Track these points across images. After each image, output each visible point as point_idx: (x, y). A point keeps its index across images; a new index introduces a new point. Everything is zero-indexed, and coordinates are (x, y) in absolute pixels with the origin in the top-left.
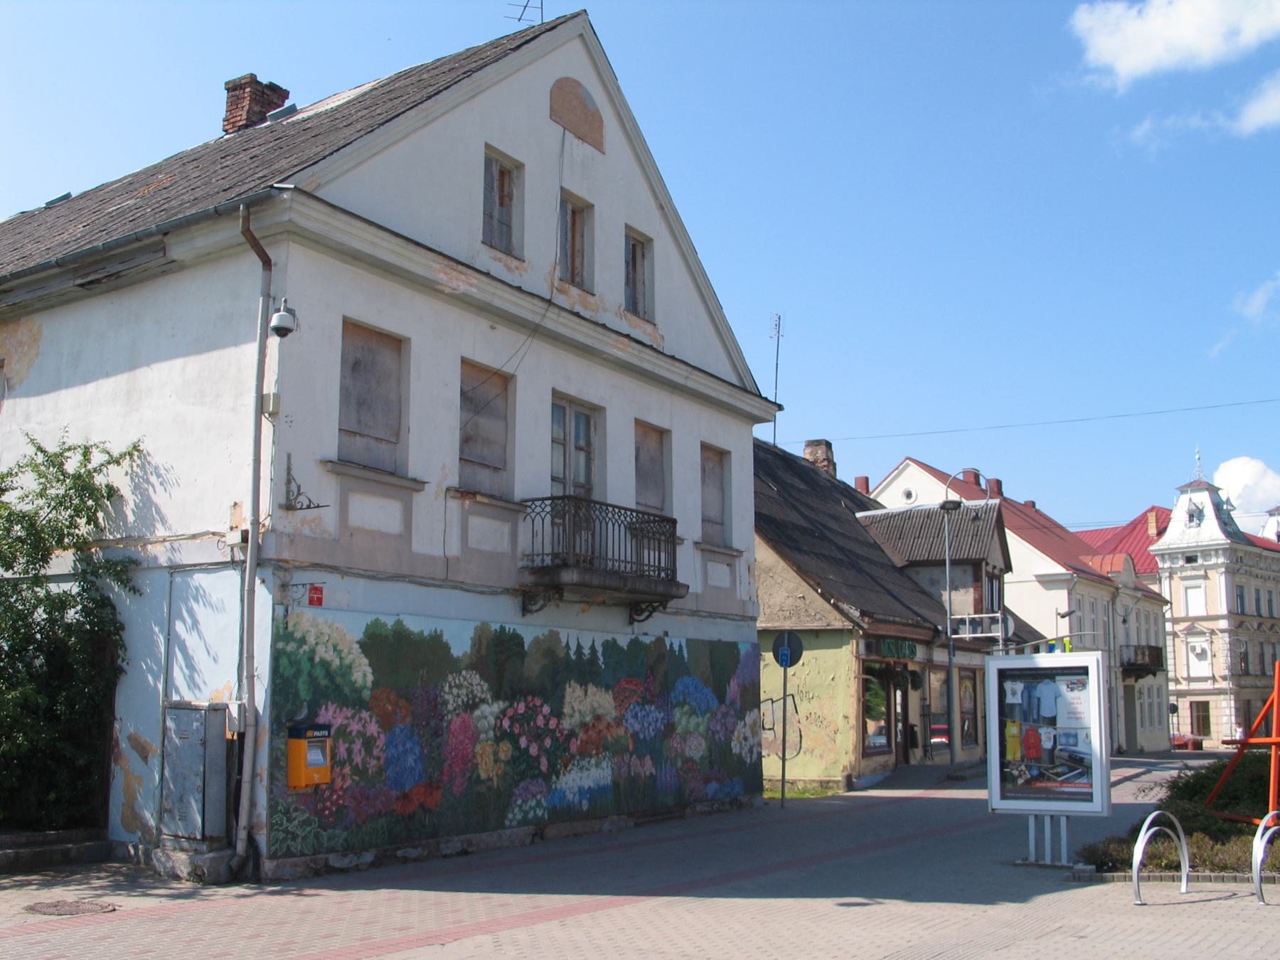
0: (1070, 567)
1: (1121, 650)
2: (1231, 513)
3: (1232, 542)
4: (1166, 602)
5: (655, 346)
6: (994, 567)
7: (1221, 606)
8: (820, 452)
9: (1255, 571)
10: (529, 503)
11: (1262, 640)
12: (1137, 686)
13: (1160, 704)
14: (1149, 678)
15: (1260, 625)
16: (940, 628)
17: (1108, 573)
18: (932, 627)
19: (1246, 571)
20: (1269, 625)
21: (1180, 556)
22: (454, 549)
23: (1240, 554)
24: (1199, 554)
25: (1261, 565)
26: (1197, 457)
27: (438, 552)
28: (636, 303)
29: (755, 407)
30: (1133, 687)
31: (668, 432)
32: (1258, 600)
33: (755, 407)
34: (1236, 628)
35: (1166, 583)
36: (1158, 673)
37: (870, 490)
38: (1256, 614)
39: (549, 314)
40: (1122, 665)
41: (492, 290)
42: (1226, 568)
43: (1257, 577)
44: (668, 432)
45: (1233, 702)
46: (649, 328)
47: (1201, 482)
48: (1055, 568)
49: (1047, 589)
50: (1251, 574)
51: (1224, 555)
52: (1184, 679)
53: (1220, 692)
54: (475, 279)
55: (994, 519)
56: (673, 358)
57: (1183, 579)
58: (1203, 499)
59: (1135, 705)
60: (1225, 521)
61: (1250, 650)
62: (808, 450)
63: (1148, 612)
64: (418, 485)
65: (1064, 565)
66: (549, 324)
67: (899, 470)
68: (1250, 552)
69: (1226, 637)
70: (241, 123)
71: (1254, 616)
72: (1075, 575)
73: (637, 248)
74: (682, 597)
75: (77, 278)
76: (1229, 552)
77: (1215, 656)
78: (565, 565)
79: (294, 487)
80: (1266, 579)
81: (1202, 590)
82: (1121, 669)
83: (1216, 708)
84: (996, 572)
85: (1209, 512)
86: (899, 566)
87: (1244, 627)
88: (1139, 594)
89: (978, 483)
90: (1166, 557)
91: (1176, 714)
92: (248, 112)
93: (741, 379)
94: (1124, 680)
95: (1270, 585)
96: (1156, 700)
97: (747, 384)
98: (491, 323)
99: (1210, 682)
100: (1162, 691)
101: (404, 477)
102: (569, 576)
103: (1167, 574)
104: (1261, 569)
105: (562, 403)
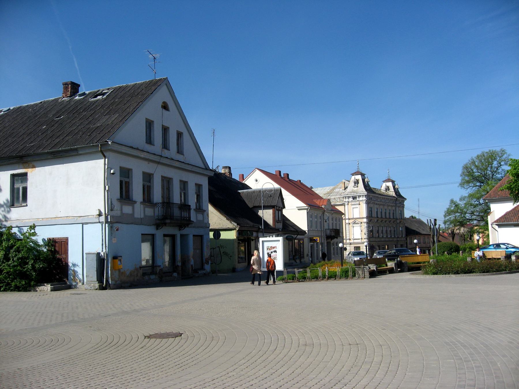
0: (307, 204)
3: (368, 193)
4: (343, 214)
5: (185, 162)
6: (279, 207)
7: (364, 214)
9: (376, 202)
10: (157, 204)
11: (378, 225)
12: (332, 242)
14: (336, 239)
15: (378, 220)
16: (260, 227)
17: (322, 205)
18: (258, 227)
19: (373, 203)
20: (381, 220)
21: (351, 197)
22: (142, 216)
23: (371, 197)
24: (357, 196)
27: (139, 217)
28: (180, 151)
29: (208, 173)
30: (330, 242)
31: (187, 182)
33: (208, 173)
35: (346, 206)
36: (338, 238)
37: (244, 179)
39: (161, 159)
40: (326, 235)
41: (149, 155)
42: (366, 201)
43: (377, 204)
44: (187, 182)
46: (182, 156)
51: (365, 197)
52: (352, 239)
53: (363, 243)
54: (145, 154)
56: (188, 164)
58: (359, 177)
59: (331, 248)
60: (367, 186)
63: (336, 217)
64: (135, 202)
66: (161, 161)
67: (253, 172)
68: (375, 196)
69: (365, 225)
70: (68, 95)
71: (375, 218)
72: (309, 207)
73: (179, 135)
74: (192, 224)
75: (52, 155)
78: (167, 219)
79: (113, 206)
80: (380, 205)
81: (358, 209)
82: (326, 237)
83: (362, 249)
84: (280, 209)
85: (361, 182)
86: (251, 207)
87: (372, 221)
88: (333, 212)
89: (280, 175)
90: (347, 197)
92: (70, 92)
93: (205, 167)
94: (327, 241)
97: (209, 174)
98: (148, 162)
99: (360, 240)
101: (133, 201)
102: (168, 221)
103: (347, 204)
104: (378, 202)
105: (163, 178)
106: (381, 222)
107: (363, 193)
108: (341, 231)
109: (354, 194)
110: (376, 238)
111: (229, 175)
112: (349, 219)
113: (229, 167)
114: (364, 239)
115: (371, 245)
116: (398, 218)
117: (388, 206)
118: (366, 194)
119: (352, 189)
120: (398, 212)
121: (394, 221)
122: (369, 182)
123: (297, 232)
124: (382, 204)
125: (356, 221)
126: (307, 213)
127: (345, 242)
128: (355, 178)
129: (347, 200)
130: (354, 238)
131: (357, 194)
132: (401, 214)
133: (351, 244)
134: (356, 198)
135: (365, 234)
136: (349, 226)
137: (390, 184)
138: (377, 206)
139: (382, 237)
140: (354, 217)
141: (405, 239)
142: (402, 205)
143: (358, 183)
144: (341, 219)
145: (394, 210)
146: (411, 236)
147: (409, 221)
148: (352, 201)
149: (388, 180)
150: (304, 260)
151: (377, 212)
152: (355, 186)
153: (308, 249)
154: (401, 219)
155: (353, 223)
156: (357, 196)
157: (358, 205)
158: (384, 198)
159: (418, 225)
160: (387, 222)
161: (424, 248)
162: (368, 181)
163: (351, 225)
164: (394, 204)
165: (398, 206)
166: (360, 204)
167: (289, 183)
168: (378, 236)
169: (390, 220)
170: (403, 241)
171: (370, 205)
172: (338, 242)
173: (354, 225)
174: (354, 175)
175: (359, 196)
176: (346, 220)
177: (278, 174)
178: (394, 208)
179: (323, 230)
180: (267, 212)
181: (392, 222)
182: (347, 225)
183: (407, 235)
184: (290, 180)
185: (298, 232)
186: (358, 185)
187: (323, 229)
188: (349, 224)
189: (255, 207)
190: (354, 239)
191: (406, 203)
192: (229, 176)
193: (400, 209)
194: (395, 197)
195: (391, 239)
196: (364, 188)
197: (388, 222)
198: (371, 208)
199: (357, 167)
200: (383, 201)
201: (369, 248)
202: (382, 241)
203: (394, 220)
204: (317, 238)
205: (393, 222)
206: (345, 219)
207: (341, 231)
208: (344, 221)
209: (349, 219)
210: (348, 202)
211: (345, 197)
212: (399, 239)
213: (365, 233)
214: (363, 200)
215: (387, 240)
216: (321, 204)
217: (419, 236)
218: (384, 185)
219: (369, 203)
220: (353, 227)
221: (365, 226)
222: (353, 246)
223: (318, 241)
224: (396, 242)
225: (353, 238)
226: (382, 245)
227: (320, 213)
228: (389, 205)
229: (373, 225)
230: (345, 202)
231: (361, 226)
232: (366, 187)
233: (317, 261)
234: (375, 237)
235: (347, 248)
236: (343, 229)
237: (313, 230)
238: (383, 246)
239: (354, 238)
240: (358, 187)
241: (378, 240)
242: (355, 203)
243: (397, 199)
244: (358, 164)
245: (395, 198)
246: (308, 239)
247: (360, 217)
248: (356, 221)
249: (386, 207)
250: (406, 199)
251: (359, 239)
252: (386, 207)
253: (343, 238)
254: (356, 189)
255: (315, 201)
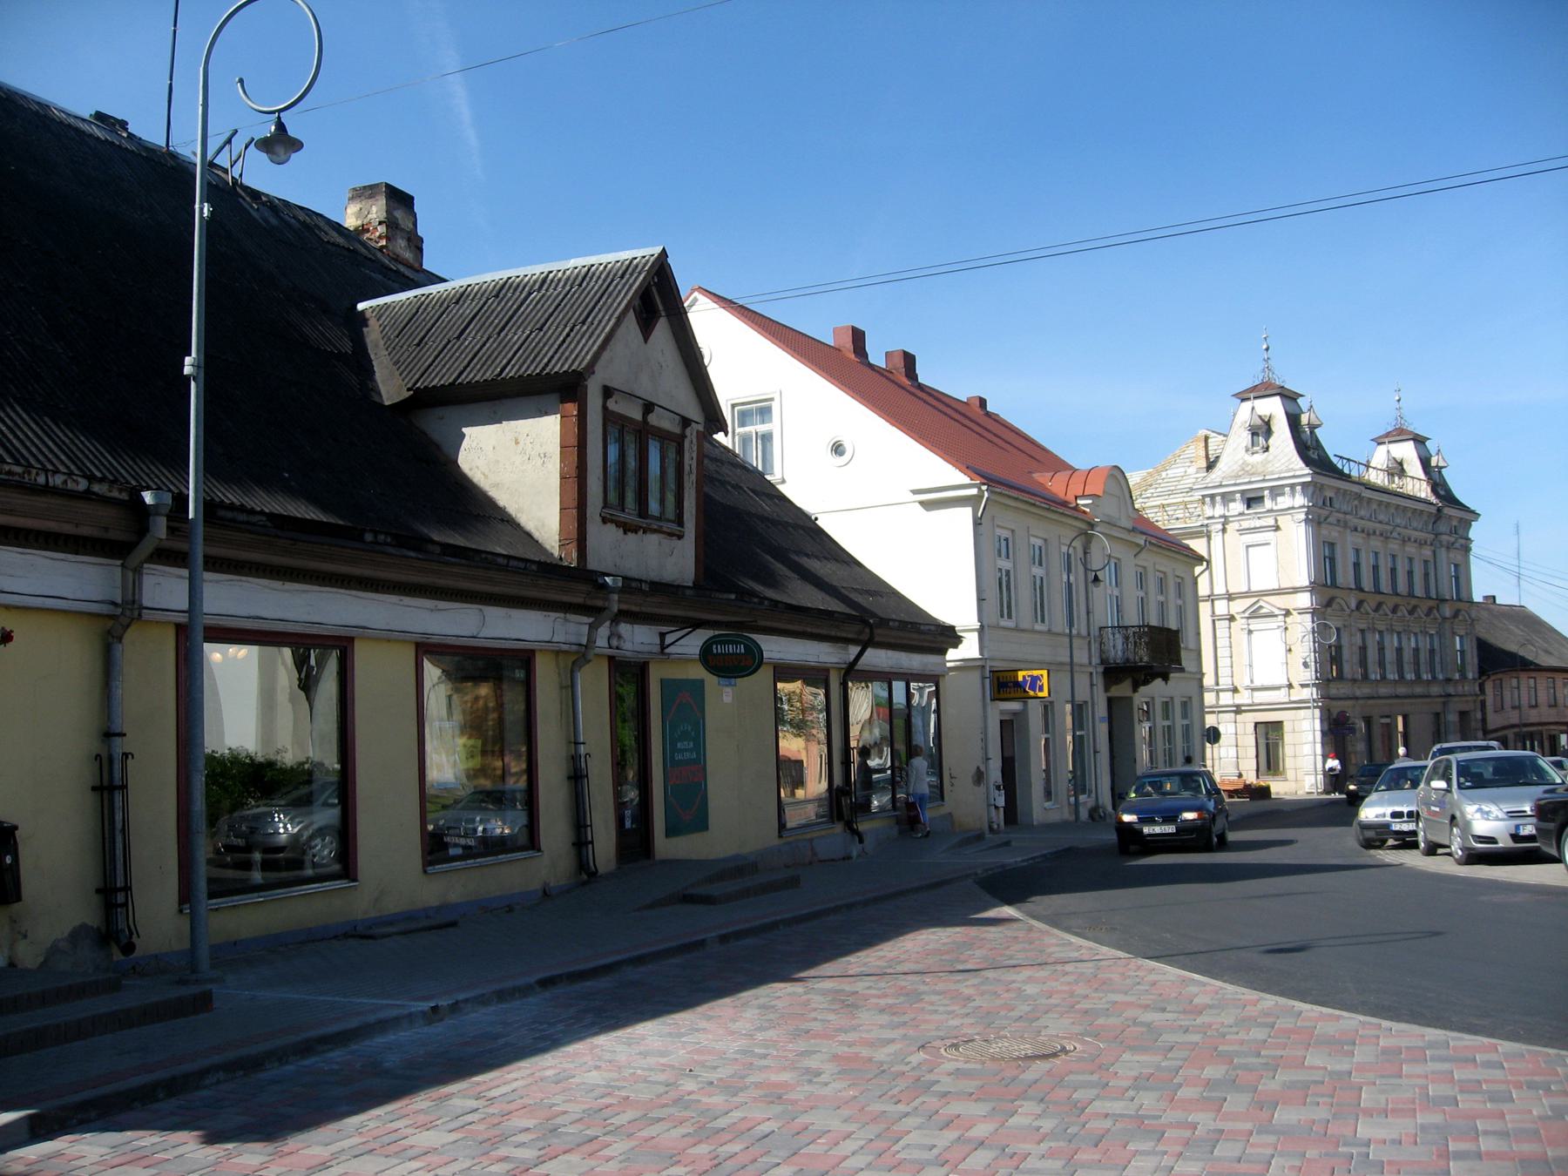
1: (1101, 635)
2: (1316, 430)
3: (1315, 473)
7: (1300, 570)
8: (374, 209)
9: (1354, 521)
13: (1187, 731)
14: (1158, 682)
15: (1360, 604)
19: (1339, 521)
20: (1374, 605)
21: (1238, 496)
23: (1329, 494)
24: (1266, 493)
25: (1362, 513)
26: (1265, 347)
32: (1357, 565)
34: (1322, 607)
35: (1217, 539)
38: (1353, 587)
42: (1307, 514)
43: (1356, 530)
45: (1318, 722)
47: (1271, 384)
48: (944, 474)
49: (927, 510)
50: (1346, 525)
53: (1298, 705)
55: (634, 288)
57: (1242, 531)
58: (1273, 407)
60: (1308, 447)
61: (1345, 642)
62: (353, 209)
65: (967, 468)
71: (1351, 589)
72: (984, 488)
76: (1311, 490)
77: (1290, 650)
80: (1369, 534)
82: (1101, 669)
87: (1335, 606)
88: (1141, 540)
91: (1217, 745)
94: (1107, 689)
95: (1376, 543)
96: (1179, 722)
99: (1284, 691)
100: (1192, 705)
103: (1220, 527)
104: (1362, 518)
106: (1376, 610)
107: (1294, 477)
108: (1187, 642)
109: (1250, 483)
110: (1354, 681)
111: (388, 238)
112: (1230, 597)
113: (387, 186)
114: (1303, 686)
115: (1335, 716)
116: (1447, 597)
117: (1405, 541)
118: (1309, 479)
119: (1241, 462)
120: (1446, 571)
121: (1430, 609)
122: (1318, 426)
123: (865, 622)
124: (1378, 533)
125: (1261, 603)
126: (977, 523)
127: (1214, 702)
128: (1253, 408)
129: (1219, 510)
130: (1252, 681)
131: (1264, 480)
132: (1457, 578)
133: (1238, 710)
134: (1260, 499)
135: (1306, 665)
136: (1230, 628)
137: (1406, 452)
138: (1358, 539)
139: (1379, 678)
140: (1253, 589)
141: (1477, 689)
142: (1462, 541)
143: (1268, 432)
144: (1188, 582)
145: (1426, 562)
146: (1500, 676)
147: (1485, 614)
148: (1241, 514)
149: (1399, 434)
150: (944, 810)
151: (1357, 565)
152: (1253, 445)
153: (985, 740)
154: (1459, 600)
155: (1246, 615)
156: (1266, 493)
157: (1272, 533)
158: (1388, 504)
159: (1522, 631)
160: (1399, 614)
161: (1552, 727)
162: (1314, 421)
163: (1240, 623)
164: (1427, 535)
165: (1445, 543)
166: (1277, 528)
167: (913, 394)
168: (1365, 677)
169: (1414, 602)
170: (1470, 698)
171: (1324, 532)
172: (1172, 698)
173: (1255, 624)
174: (1249, 399)
175: (1276, 492)
176: (1216, 602)
177: (850, 346)
178: (1427, 552)
179: (1084, 632)
180: (522, 439)
181: (1420, 612)
182: (1222, 626)
183: (1483, 671)
184: (921, 387)
185: (871, 626)
186: (1271, 441)
187: (1084, 623)
188: (1232, 619)
189: (424, 399)
190: (1253, 690)
191: (1475, 532)
192: (383, 242)
193: (1452, 555)
194: (1432, 504)
195: (1419, 690)
196: (1295, 452)
197: (1403, 611)
198: (1332, 545)
199: (1262, 365)
200: (1381, 517)
201: (1326, 728)
202: (1380, 698)
203: (1431, 603)
204: (1035, 673)
205: (1427, 615)
206: (1212, 598)
207: (1192, 645)
208: (1204, 609)
209: (1230, 597)
210: (1226, 521)
211: (1208, 500)
212: (1451, 690)
213: (1308, 660)
214: (1293, 508)
215: (1402, 690)
216: (1076, 489)
217: (1533, 674)
218: (1380, 457)
219: (1319, 523)
220: (1250, 632)
221: (1303, 625)
222: (1250, 719)
223: (1041, 689)
224: (1442, 700)
225: (1247, 682)
226: (1382, 717)
227: (1062, 537)
228: (1409, 539)
229: (1340, 624)
230: (1209, 518)
231: (1286, 629)
232: (1307, 448)
233: (1047, 804)
234: (1349, 677)
235: (1222, 729)
236: (1198, 634)
237: (1017, 629)
238: (1387, 720)
239: (1252, 681)
240: (1267, 449)
241: (1366, 690)
242: (1258, 523)
243: (1439, 510)
244: (1267, 349)
245: (1433, 510)
246: (983, 678)
247: (1282, 586)
248: (1261, 603)
249: (1394, 546)
250: (1479, 515)
251: (1278, 688)
252: (1394, 546)
253: (1201, 680)
254: (1259, 457)
255: (1041, 480)
